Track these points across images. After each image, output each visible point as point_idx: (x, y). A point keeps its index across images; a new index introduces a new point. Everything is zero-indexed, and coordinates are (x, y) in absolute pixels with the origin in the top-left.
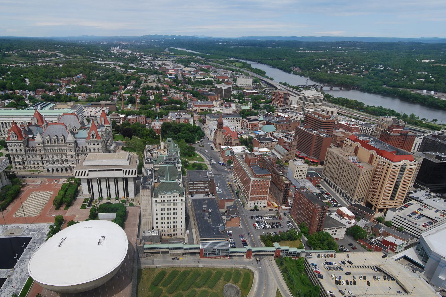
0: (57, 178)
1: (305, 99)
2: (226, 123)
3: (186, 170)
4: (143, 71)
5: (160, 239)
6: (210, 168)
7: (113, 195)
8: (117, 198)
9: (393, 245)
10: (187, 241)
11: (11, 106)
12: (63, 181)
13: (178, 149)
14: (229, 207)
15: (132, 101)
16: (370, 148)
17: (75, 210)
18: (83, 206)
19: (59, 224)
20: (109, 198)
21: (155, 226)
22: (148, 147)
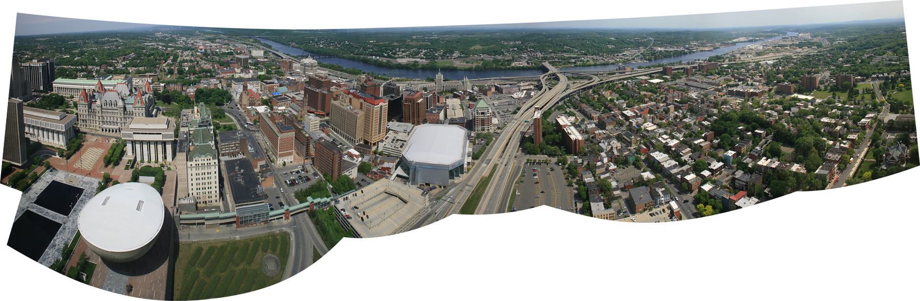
0: (109, 138)
1: (305, 65)
2: (249, 87)
3: (218, 131)
4: (179, 48)
5: (196, 208)
6: (239, 127)
7: (153, 160)
8: (157, 161)
9: (388, 169)
10: (222, 209)
11: (84, 77)
12: (113, 141)
13: (209, 112)
14: (262, 166)
15: (171, 72)
16: (359, 97)
17: (118, 171)
18: (127, 168)
19: (107, 182)
20: (150, 161)
21: (190, 193)
22: (184, 111)
